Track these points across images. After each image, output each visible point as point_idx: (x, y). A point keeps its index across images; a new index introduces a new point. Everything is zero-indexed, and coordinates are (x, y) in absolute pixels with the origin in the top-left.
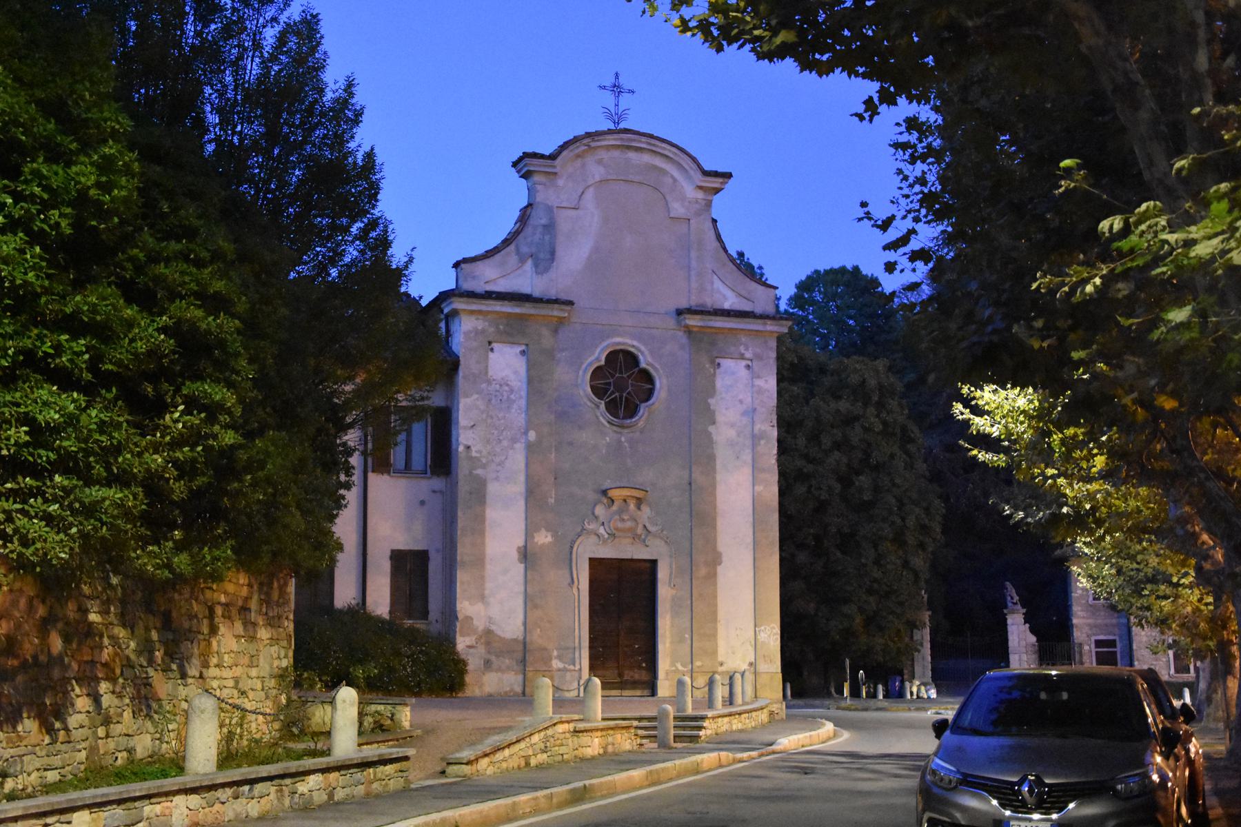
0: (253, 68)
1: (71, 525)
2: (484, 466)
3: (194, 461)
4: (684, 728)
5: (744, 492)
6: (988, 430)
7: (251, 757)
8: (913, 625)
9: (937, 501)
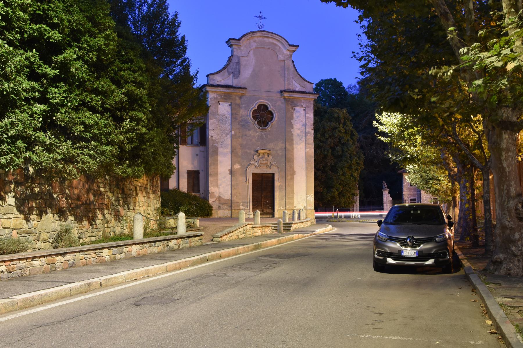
0: (145, 9)
1: (97, 158)
2: (217, 143)
3: (132, 138)
4: (286, 227)
5: (302, 151)
6: (384, 130)
7: (151, 234)
8: (353, 195)
9: (362, 155)
